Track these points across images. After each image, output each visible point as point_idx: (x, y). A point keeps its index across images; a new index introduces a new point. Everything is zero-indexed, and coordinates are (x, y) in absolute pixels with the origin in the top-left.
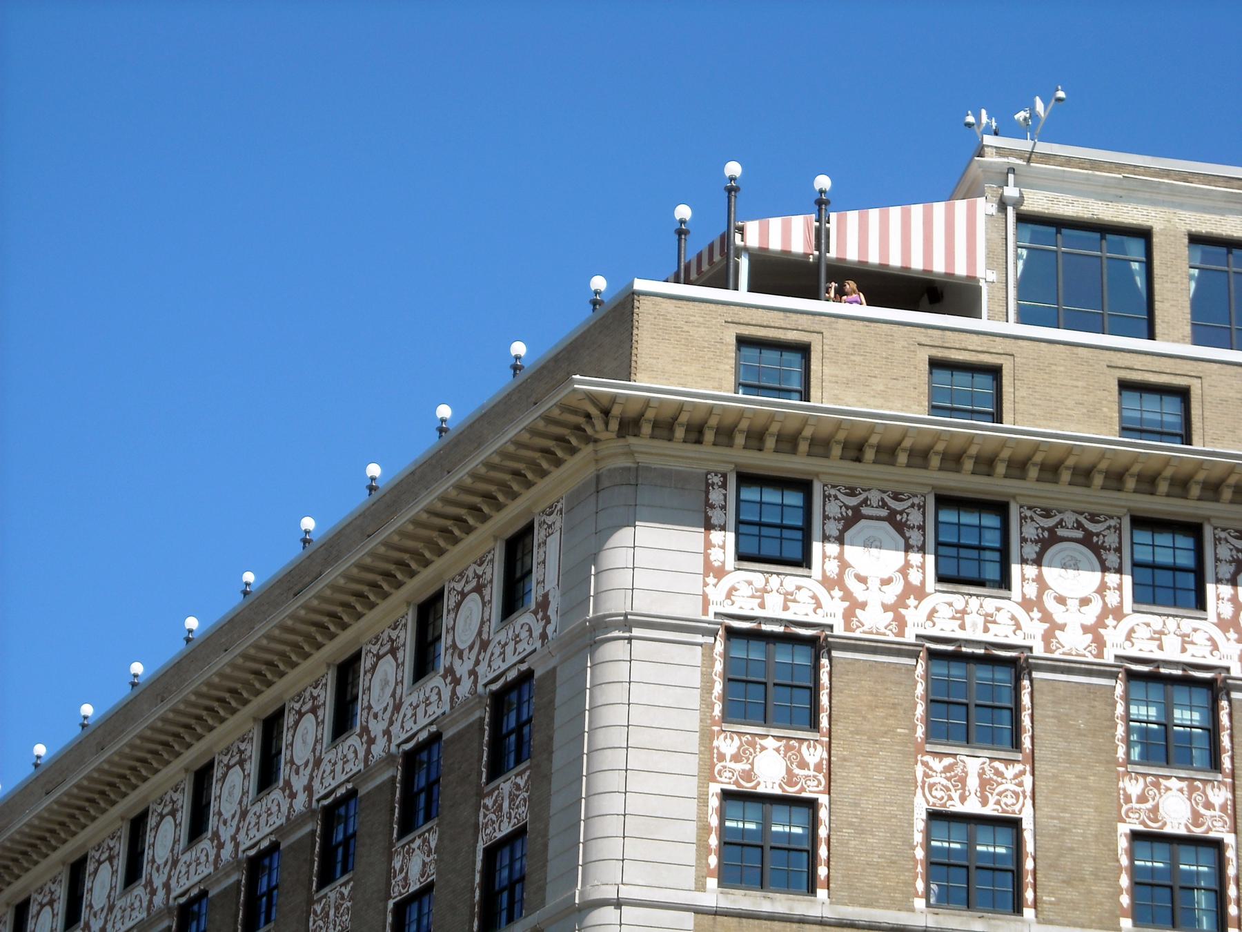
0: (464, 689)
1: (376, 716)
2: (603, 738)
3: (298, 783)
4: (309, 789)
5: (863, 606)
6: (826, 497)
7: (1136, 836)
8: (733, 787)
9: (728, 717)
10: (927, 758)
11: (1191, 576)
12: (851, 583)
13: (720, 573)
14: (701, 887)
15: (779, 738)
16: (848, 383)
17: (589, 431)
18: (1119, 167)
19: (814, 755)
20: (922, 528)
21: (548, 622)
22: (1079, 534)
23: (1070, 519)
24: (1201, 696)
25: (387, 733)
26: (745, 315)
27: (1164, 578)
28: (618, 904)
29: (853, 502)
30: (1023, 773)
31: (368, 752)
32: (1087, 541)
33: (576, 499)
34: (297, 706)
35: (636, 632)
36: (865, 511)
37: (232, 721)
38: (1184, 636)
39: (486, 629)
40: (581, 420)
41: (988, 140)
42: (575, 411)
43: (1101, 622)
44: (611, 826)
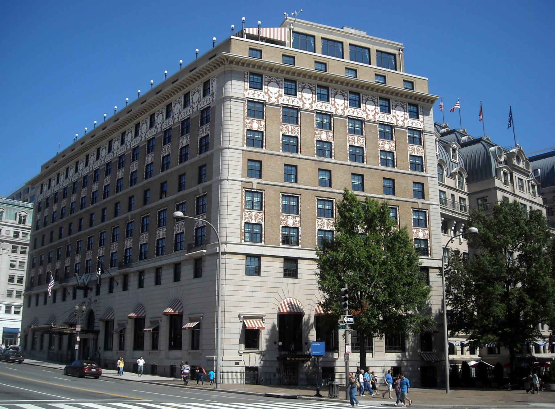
0: (195, 110)
1: (175, 114)
2: (225, 119)
3: (159, 126)
4: (161, 127)
5: (272, 97)
6: (265, 78)
7: (317, 141)
8: (249, 129)
9: (248, 116)
10: (282, 125)
11: (327, 96)
13: (247, 90)
14: (243, 146)
15: (257, 120)
16: (268, 57)
17: (224, 63)
18: (310, 24)
19: (263, 124)
20: (282, 84)
22: (309, 87)
23: (307, 84)
24: (328, 117)
25: (178, 117)
26: (251, 44)
27: (322, 96)
28: (229, 148)
29: (270, 79)
30: (299, 129)
32: (310, 88)
33: (219, 76)
34: (158, 113)
35: (232, 100)
36: (338, 93)
37: (144, 115)
38: (326, 106)
39: (200, 99)
40: (222, 61)
41: (288, 17)
42: (221, 59)
44: (228, 135)
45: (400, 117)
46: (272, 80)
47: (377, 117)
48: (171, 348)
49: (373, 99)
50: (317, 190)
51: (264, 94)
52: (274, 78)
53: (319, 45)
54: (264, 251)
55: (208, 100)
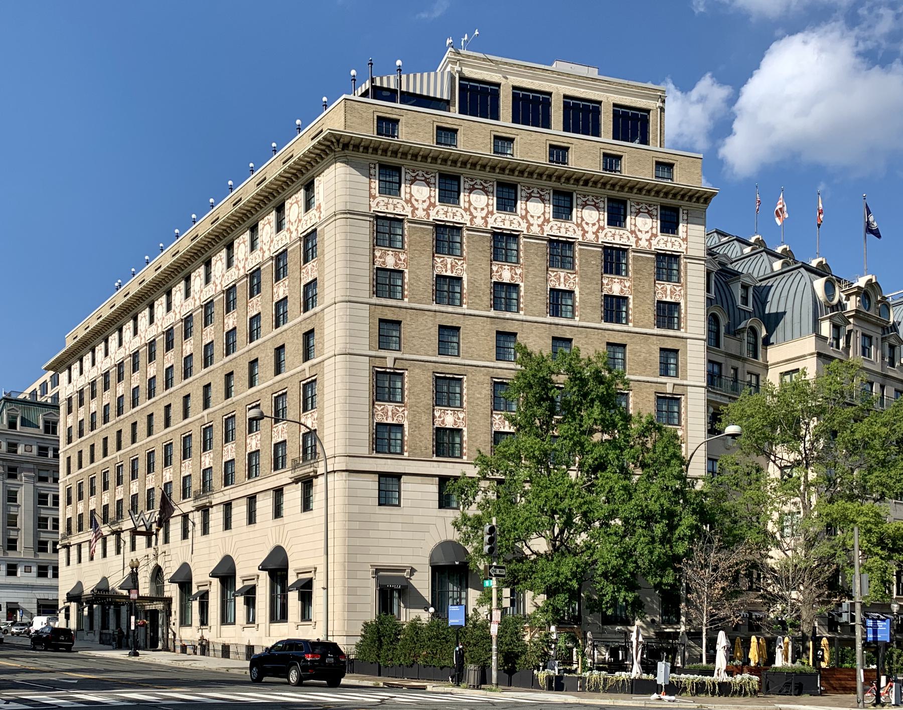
4: (244, 267)
12: (529, 218)
13: (375, 197)
17: (333, 148)
21: (321, 213)
25: (269, 249)
29: (414, 174)
31: (263, 256)
36: (533, 195)
43: (487, 216)
45: (644, 232)
46: (418, 178)
47: (490, 220)
48: (273, 619)
49: (596, 203)
50: (493, 368)
51: (463, 212)
52: (536, 191)
53: (557, 114)
54: (407, 467)
55: (313, 217)
